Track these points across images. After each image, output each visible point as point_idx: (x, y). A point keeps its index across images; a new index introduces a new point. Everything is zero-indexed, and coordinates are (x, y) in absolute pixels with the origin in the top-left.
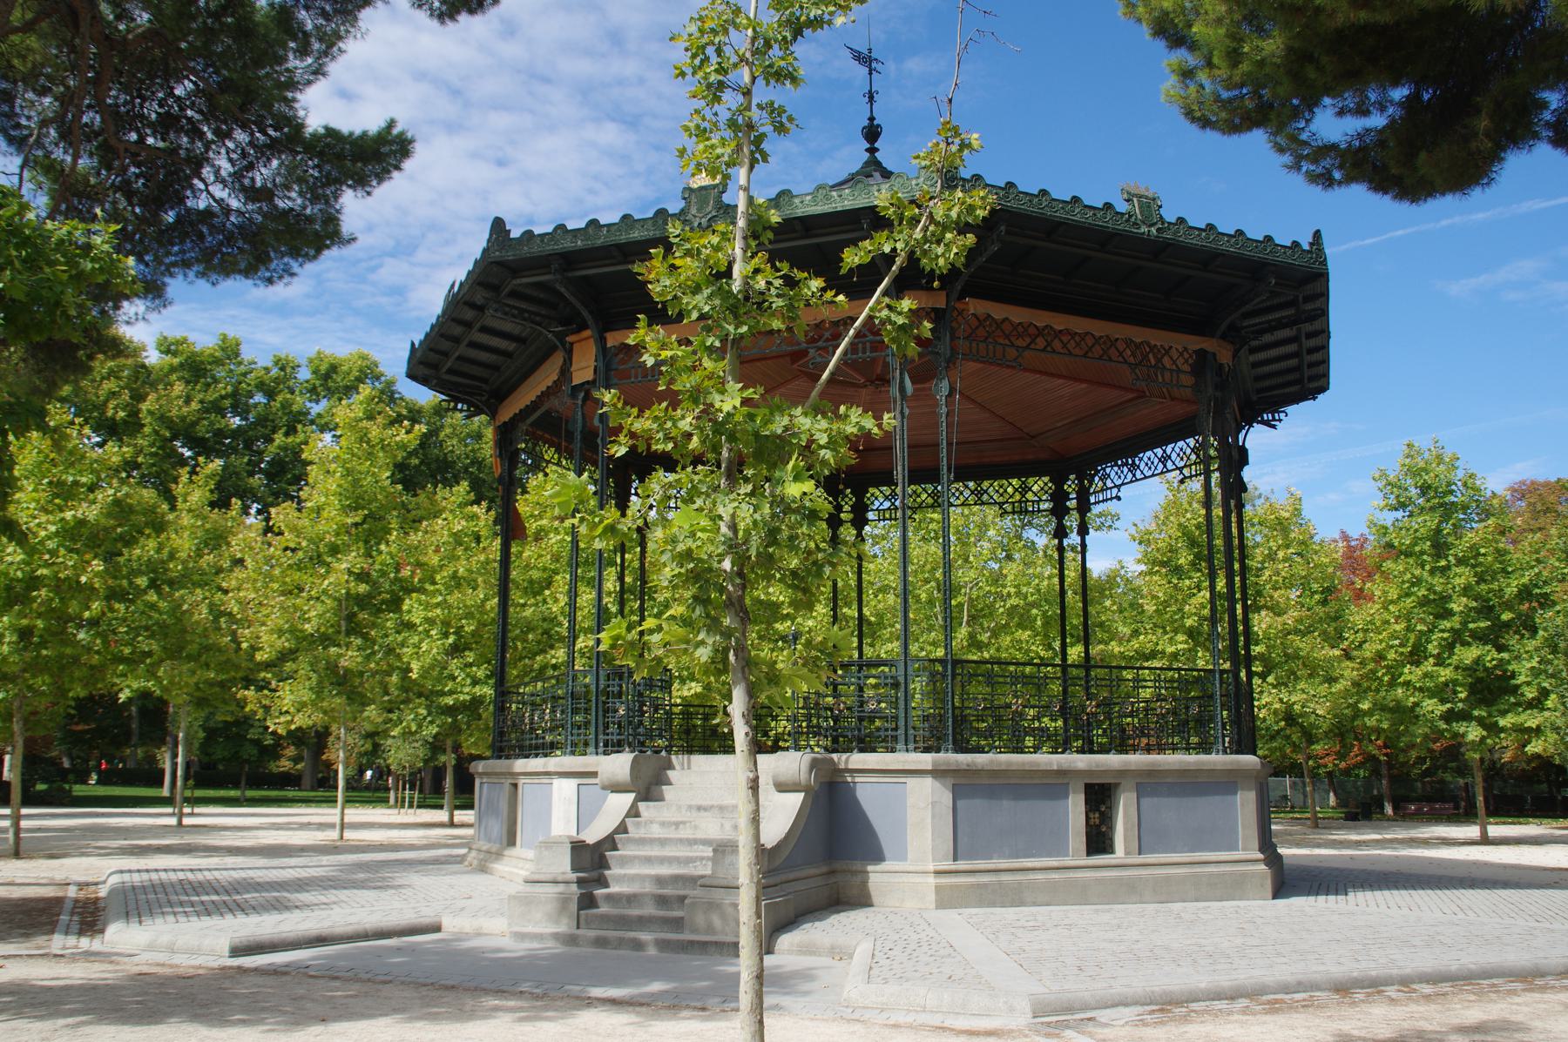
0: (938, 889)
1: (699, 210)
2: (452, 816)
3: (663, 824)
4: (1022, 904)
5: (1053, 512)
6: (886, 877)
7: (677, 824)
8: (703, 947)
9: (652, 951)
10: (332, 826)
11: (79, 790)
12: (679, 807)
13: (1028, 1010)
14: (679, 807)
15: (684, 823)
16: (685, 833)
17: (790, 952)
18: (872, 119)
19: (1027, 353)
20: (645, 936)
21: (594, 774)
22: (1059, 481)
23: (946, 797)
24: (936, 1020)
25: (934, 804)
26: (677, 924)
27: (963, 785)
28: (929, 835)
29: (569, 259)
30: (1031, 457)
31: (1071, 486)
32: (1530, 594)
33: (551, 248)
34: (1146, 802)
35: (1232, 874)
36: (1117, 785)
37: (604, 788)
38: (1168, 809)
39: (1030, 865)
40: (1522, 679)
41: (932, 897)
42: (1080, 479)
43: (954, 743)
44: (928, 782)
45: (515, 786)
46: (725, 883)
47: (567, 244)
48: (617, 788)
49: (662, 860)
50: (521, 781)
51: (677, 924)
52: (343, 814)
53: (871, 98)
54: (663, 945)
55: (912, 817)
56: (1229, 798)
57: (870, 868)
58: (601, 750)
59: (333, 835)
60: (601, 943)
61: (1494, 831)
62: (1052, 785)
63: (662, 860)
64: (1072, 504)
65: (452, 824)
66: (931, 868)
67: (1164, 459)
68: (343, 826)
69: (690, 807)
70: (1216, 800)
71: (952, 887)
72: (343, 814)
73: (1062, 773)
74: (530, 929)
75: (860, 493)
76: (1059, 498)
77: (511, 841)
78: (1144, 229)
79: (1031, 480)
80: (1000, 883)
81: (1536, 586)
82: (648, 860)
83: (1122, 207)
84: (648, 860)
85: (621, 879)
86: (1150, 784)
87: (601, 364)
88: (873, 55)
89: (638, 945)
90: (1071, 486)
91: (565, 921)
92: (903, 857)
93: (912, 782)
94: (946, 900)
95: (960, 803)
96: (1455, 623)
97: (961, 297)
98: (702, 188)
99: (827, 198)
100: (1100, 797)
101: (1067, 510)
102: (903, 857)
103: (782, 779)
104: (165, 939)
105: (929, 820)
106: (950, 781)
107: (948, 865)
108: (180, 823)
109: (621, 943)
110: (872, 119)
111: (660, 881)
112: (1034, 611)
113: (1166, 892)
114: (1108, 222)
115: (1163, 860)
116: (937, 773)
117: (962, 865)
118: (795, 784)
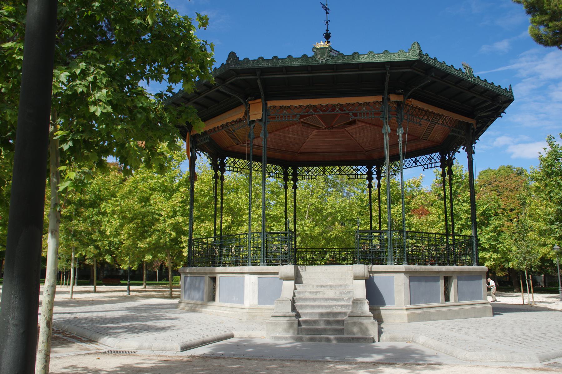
0: (408, 315)
1: (321, 57)
2: (95, 288)
3: (310, 292)
4: (430, 320)
5: (367, 179)
6: (387, 311)
7: (316, 293)
8: (358, 340)
9: (334, 342)
10: (68, 292)
11: (122, 282)
12: (313, 286)
13: (537, 359)
14: (313, 286)
15: (319, 292)
16: (319, 296)
17: (386, 341)
18: (327, 30)
19: (422, 120)
20: (332, 337)
21: (277, 273)
22: (370, 168)
23: (408, 281)
24: (504, 364)
25: (404, 283)
26: (342, 331)
27: (413, 277)
28: (403, 295)
29: (264, 71)
30: (342, 159)
31: (290, 171)
32: (485, 213)
33: (257, 66)
34: (459, 282)
35: (483, 308)
36: (451, 276)
37: (281, 279)
38: (467, 285)
39: (431, 306)
40: (483, 241)
41: (406, 318)
42: (378, 167)
43: (407, 261)
44: (402, 276)
45: (214, 279)
46: (358, 315)
47: (265, 65)
48: (287, 279)
49: (319, 307)
50: (218, 277)
51: (342, 331)
52: (72, 288)
53: (327, 23)
54: (339, 340)
55: (396, 289)
56: (480, 281)
57: (381, 308)
58: (265, 264)
59: (68, 296)
60: (312, 340)
61: (99, 288)
62: (433, 277)
63: (319, 307)
64: (375, 176)
65: (95, 291)
66: (405, 307)
67: (416, 162)
68: (73, 292)
69: (318, 286)
70: (477, 281)
71: (413, 314)
72: (72, 288)
73: (439, 272)
74: (277, 335)
75: (295, 169)
76: (370, 174)
77: (213, 298)
78: (470, 79)
79: (326, 168)
80: (424, 312)
81: (487, 210)
82: (313, 307)
83: (464, 71)
84: (313, 307)
85: (306, 314)
86: (461, 276)
87: (264, 113)
88: (328, 7)
89: (328, 340)
90: (374, 169)
91: (291, 331)
92: (393, 304)
93: (396, 276)
94: (411, 319)
95: (411, 283)
96: (463, 222)
97: (409, 98)
98: (321, 48)
99: (373, 56)
100: (447, 280)
101: (373, 178)
102: (393, 304)
103: (358, 275)
104: (146, 344)
105: (403, 290)
106: (408, 275)
107: (409, 306)
108: (171, 294)
109: (320, 340)
110: (327, 30)
111: (322, 315)
112: (339, 214)
113: (467, 315)
114: (461, 75)
115: (465, 303)
116: (405, 273)
117: (260, 307)
118: (362, 277)
